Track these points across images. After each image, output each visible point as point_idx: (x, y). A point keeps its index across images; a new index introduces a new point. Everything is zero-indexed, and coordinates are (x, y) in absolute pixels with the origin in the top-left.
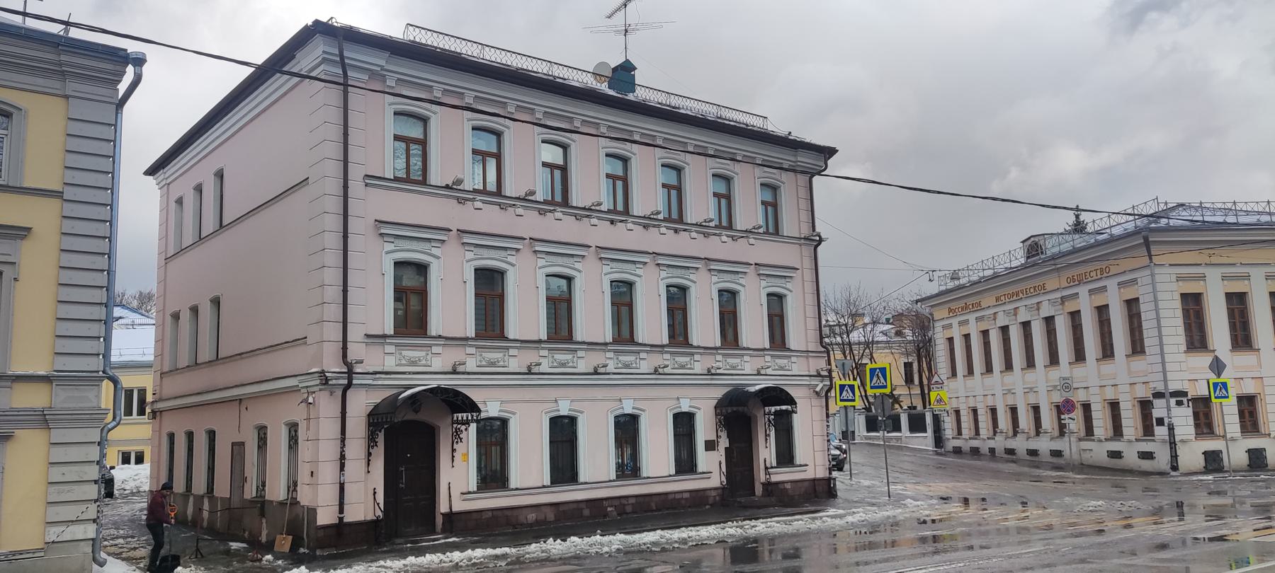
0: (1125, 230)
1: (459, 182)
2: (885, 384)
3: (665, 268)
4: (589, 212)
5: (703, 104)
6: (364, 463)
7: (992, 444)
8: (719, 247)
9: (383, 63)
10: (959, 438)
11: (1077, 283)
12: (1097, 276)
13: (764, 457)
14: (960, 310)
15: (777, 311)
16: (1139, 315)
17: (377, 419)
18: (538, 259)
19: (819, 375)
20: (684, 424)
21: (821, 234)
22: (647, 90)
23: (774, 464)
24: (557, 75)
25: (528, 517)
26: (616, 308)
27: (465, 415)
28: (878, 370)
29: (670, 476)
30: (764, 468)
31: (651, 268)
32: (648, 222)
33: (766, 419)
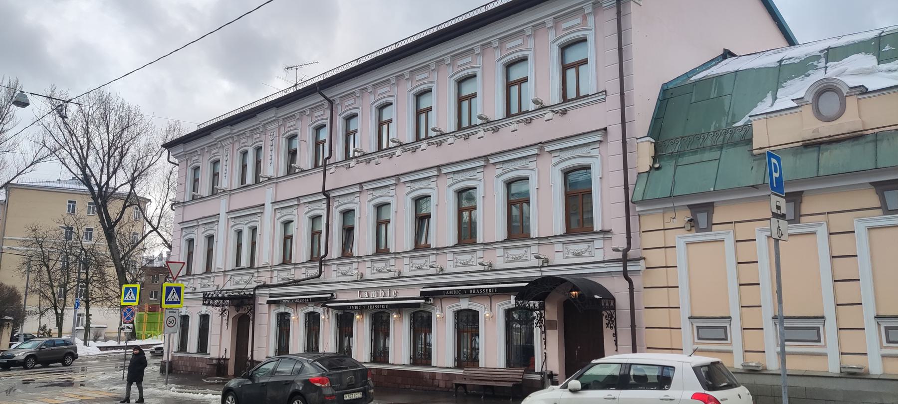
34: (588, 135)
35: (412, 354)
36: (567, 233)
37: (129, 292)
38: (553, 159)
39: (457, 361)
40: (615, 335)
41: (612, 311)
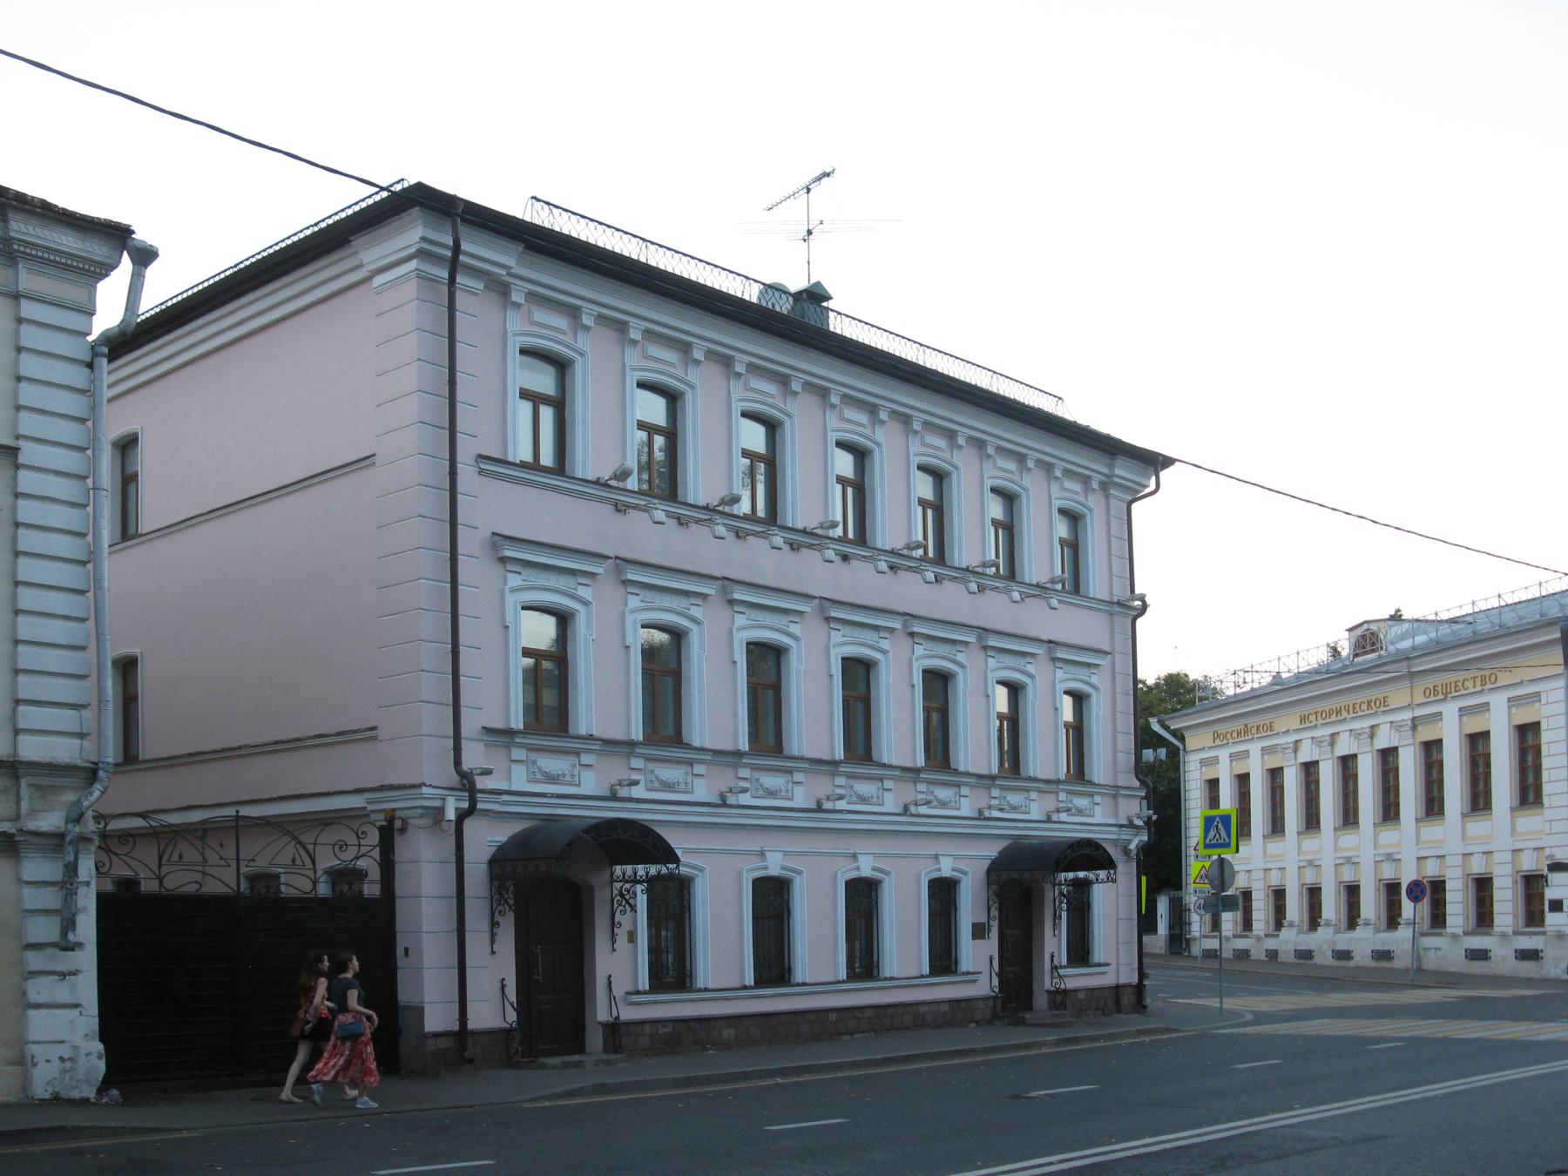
0: (1521, 618)
2: (1227, 840)
4: (805, 539)
6: (487, 936)
7: (1271, 944)
8: (997, 609)
9: (510, 261)
10: (1246, 937)
11: (1441, 697)
12: (1475, 687)
13: (1051, 952)
14: (1235, 735)
16: (1537, 750)
17: (502, 863)
18: (736, 615)
19: (1131, 825)
20: (943, 893)
21: (1146, 599)
23: (1064, 961)
25: (723, 1033)
28: (1218, 819)
29: (922, 976)
30: (1050, 967)
32: (898, 561)
33: (1057, 892)
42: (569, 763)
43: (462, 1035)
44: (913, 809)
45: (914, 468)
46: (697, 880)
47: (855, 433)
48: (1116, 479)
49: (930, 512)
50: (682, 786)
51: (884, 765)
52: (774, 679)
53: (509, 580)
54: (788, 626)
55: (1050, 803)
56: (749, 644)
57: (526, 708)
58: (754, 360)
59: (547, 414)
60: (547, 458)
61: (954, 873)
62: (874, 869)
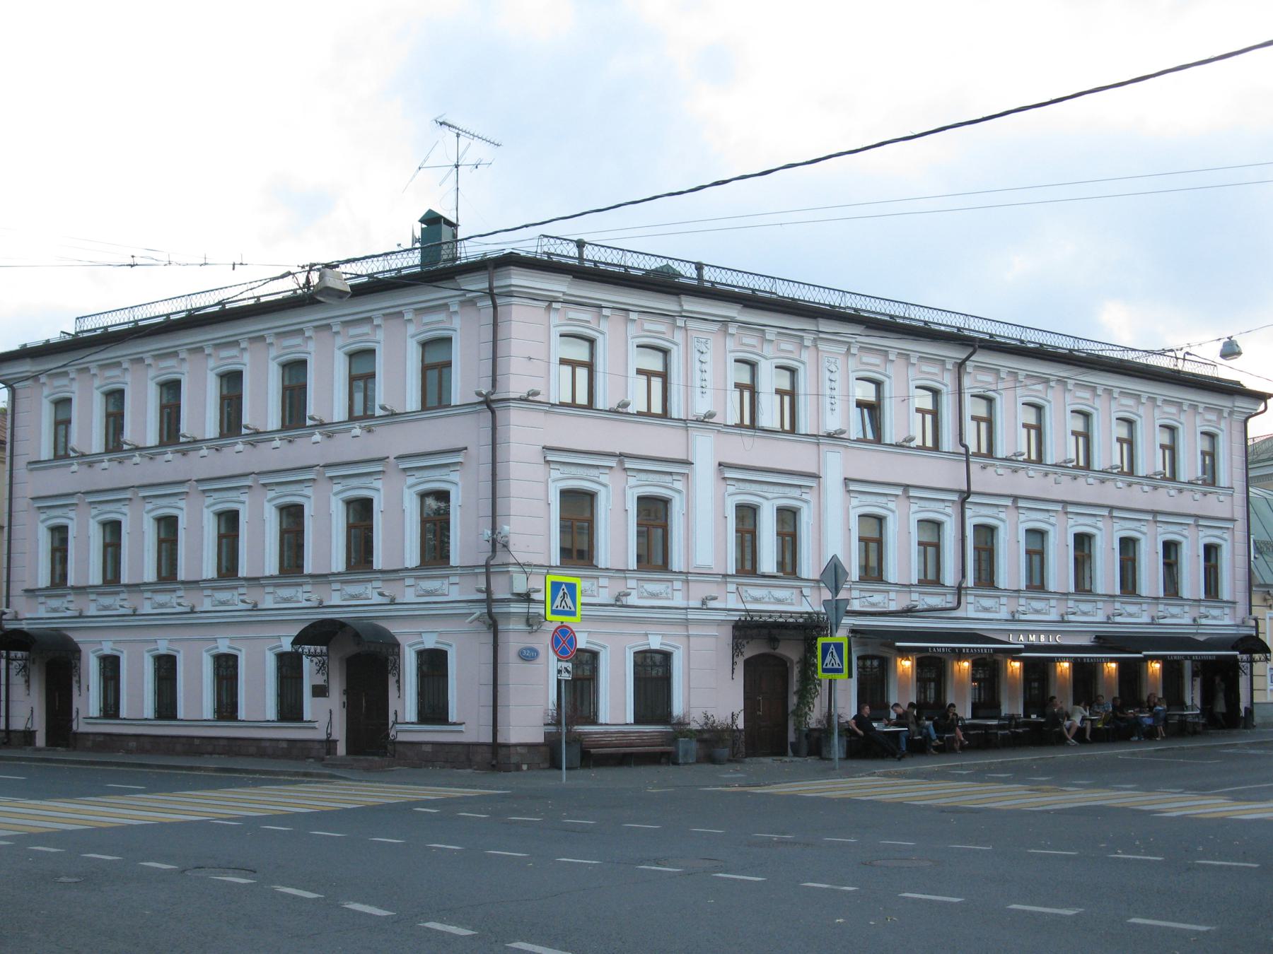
1: (626, 405)
3: (1024, 511)
5: (997, 324)
15: (788, 529)
22: (930, 311)
24: (630, 265)
26: (863, 543)
27: (312, 647)
31: (619, 475)
34: (435, 456)
35: (102, 706)
36: (421, 565)
37: (561, 593)
38: (147, 505)
39: (217, 712)
40: (398, 681)
41: (396, 657)
42: (664, 586)
43: (496, 747)
44: (1017, 616)
45: (1114, 420)
46: (601, 654)
47: (1171, 419)
48: (1236, 409)
49: (1167, 452)
50: (664, 595)
51: (1098, 595)
52: (751, 527)
53: (1020, 518)
54: (887, 504)
55: (618, 587)
56: (1075, 535)
57: (860, 567)
58: (976, 364)
59: (983, 426)
60: (929, 443)
61: (588, 645)
62: (437, 642)
